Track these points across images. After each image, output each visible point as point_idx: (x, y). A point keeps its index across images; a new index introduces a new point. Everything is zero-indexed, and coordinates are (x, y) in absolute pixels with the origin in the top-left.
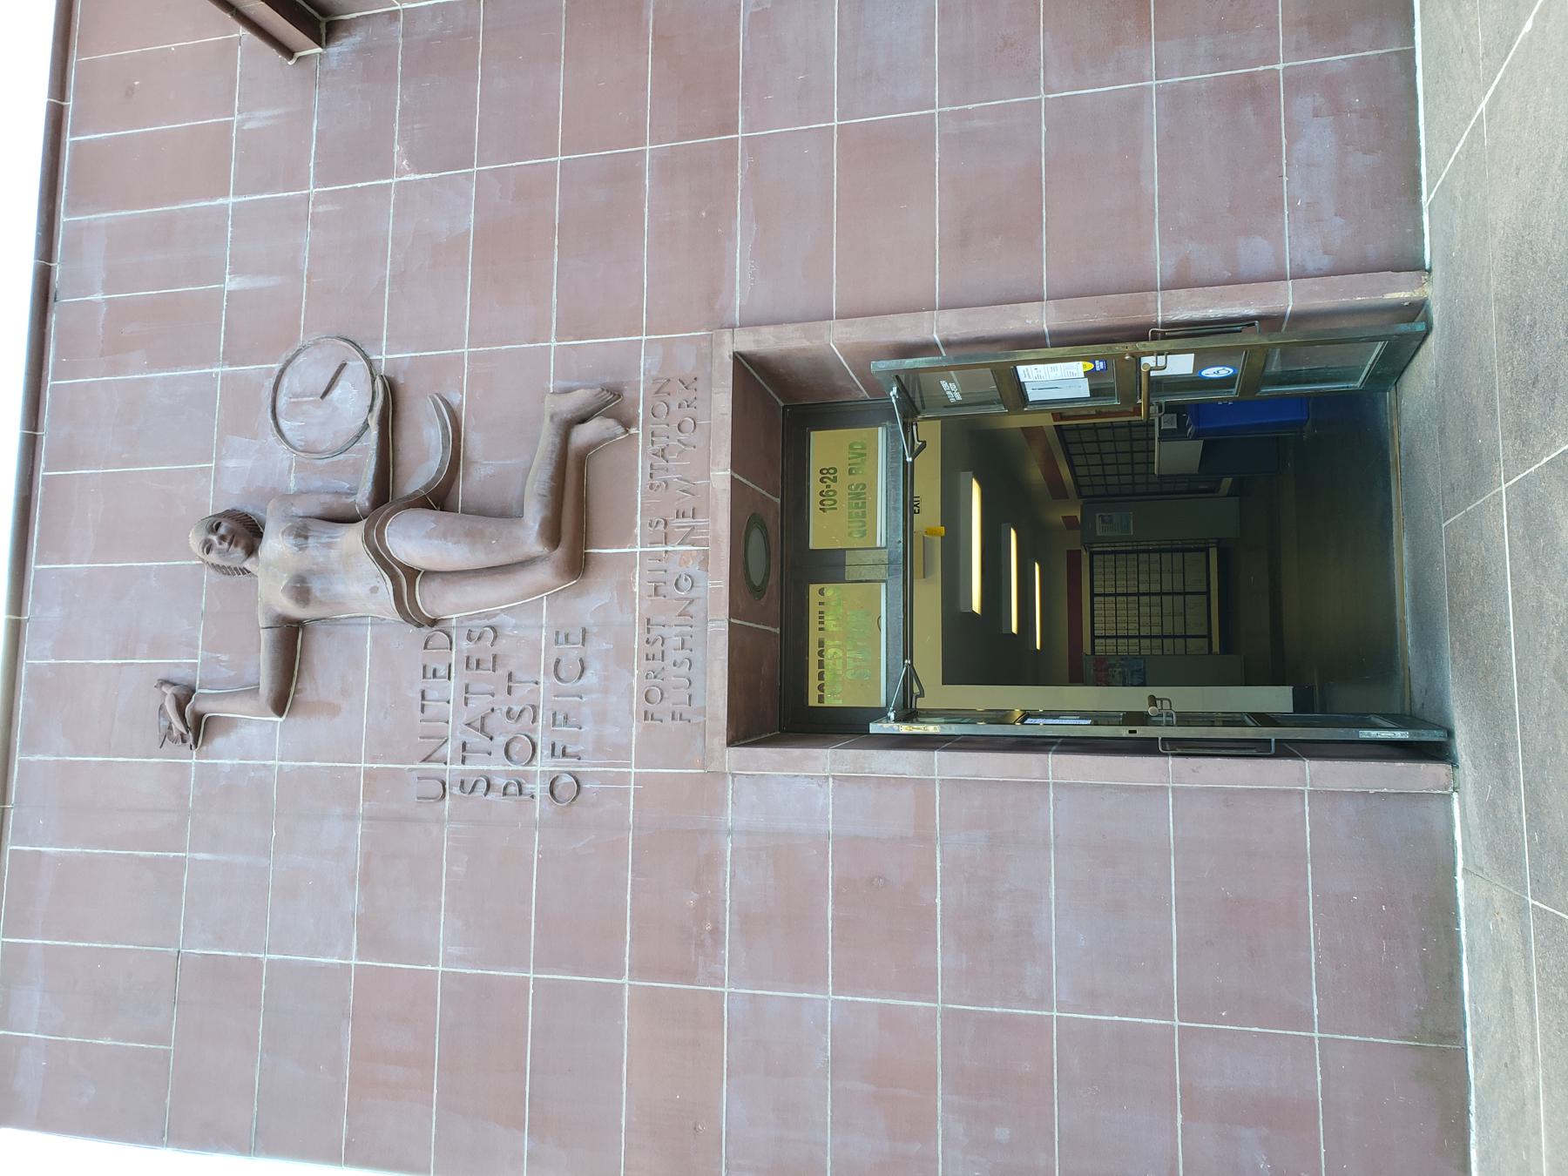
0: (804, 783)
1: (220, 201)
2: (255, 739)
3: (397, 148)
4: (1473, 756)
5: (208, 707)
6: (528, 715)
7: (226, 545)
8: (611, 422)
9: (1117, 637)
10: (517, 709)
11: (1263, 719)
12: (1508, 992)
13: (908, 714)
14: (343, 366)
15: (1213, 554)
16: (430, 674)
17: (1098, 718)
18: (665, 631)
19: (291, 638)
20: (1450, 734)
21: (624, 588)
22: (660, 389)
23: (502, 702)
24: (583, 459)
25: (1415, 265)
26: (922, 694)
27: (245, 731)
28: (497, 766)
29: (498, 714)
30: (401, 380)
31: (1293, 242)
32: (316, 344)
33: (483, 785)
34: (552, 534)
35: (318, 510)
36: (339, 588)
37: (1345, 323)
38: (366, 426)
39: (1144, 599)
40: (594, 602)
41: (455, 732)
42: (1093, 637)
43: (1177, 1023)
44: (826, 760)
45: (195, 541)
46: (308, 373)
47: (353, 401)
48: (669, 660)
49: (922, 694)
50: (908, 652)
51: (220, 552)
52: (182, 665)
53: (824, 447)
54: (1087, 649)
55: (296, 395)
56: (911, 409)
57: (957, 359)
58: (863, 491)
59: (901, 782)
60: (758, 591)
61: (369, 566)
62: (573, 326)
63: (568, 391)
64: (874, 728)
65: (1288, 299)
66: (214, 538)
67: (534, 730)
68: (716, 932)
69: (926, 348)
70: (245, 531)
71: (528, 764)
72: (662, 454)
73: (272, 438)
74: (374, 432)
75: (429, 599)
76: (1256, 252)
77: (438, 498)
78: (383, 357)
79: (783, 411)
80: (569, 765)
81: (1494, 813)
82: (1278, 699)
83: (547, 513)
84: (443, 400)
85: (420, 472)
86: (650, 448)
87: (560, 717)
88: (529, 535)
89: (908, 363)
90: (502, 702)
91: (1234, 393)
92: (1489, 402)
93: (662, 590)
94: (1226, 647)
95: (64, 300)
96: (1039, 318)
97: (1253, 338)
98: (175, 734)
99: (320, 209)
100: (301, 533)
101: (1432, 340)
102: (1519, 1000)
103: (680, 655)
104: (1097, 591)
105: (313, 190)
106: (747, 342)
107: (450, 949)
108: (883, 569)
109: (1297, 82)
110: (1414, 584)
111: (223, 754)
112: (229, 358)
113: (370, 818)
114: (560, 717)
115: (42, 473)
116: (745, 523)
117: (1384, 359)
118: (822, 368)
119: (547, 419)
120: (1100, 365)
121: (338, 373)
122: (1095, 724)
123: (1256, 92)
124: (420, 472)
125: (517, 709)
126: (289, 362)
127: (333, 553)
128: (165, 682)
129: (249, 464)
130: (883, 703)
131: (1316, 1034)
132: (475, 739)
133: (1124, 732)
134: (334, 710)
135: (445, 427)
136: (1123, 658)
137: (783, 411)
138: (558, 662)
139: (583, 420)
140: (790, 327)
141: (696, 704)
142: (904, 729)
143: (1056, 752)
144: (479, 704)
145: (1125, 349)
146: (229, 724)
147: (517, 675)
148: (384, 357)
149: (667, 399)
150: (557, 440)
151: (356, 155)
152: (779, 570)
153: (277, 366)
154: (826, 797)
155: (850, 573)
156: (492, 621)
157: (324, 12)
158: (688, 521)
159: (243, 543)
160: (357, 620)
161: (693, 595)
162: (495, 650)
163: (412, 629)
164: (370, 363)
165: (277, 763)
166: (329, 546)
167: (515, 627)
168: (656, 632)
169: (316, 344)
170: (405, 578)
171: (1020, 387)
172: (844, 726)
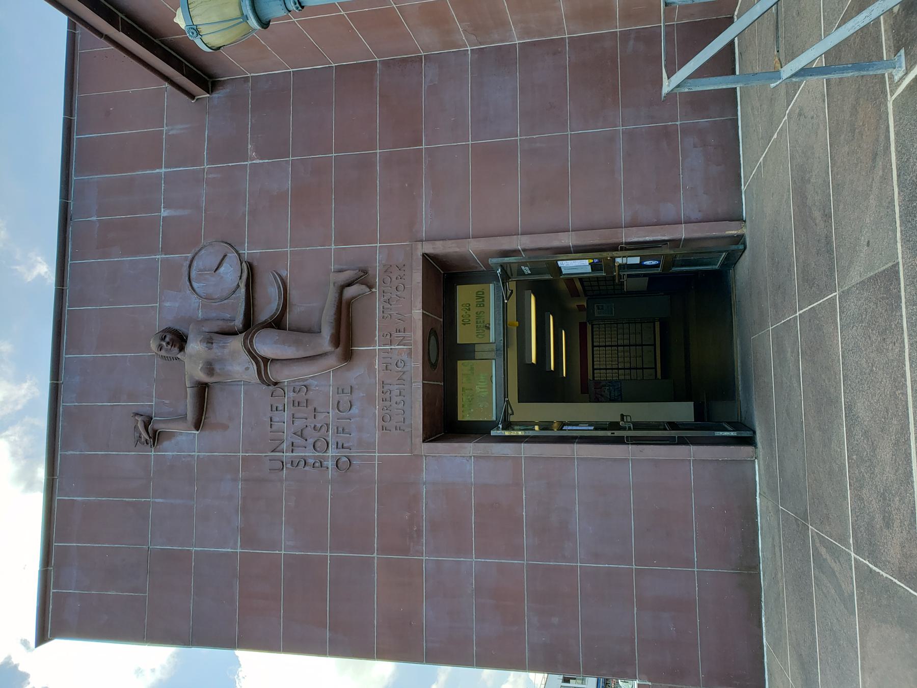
0: (461, 459)
1: (158, 171)
2: (185, 443)
3: (250, 146)
4: (762, 443)
5: (160, 427)
6: (324, 429)
7: (169, 347)
8: (364, 287)
9: (606, 369)
10: (319, 425)
11: (673, 426)
12: (774, 546)
13: (508, 425)
14: (225, 256)
15: (657, 324)
16: (274, 409)
17: (598, 427)
18: (391, 387)
19: (202, 391)
20: (754, 432)
21: (371, 366)
22: (387, 270)
23: (311, 422)
24: (349, 303)
25: (740, 219)
26: (513, 414)
27: (179, 438)
28: (309, 453)
29: (309, 428)
30: (255, 264)
31: (685, 206)
32: (211, 244)
33: (302, 463)
34: (336, 341)
35: (216, 330)
36: (229, 368)
37: (710, 244)
38: (238, 286)
39: (620, 348)
40: (356, 373)
41: (288, 437)
42: (594, 369)
43: (634, 567)
44: (470, 448)
45: (153, 346)
46: (207, 259)
47: (231, 273)
48: (393, 401)
49: (513, 414)
50: (506, 395)
51: (166, 350)
52: (148, 404)
53: (464, 294)
54: (590, 377)
55: (201, 270)
56: (506, 277)
57: (530, 258)
58: (482, 314)
59: (506, 458)
60: (434, 366)
61: (245, 357)
62: (342, 239)
63: (341, 271)
64: (493, 433)
65: (682, 232)
66: (164, 344)
67: (328, 436)
68: (419, 532)
69: (515, 252)
70: (179, 339)
71: (325, 452)
72: (388, 301)
73: (189, 291)
74: (243, 290)
75: (274, 373)
76: (668, 210)
77: (277, 323)
78: (246, 252)
79: (445, 278)
80: (346, 452)
81: (768, 468)
82: (684, 411)
83: (333, 331)
84: (280, 276)
85: (268, 308)
86: (382, 299)
87: (340, 429)
88: (325, 341)
89: (507, 260)
90: (311, 422)
91: (659, 270)
92: (766, 289)
93: (389, 367)
94: (665, 375)
95: (76, 220)
96: (567, 240)
97: (666, 251)
98: (143, 440)
99: (210, 176)
100: (209, 341)
101: (747, 252)
102: (777, 549)
103: (399, 399)
104: (595, 344)
105: (206, 166)
106: (429, 248)
107: (288, 543)
108: (494, 353)
109: (686, 130)
110: (742, 362)
111: (168, 450)
112: (165, 251)
113: (245, 480)
114: (340, 429)
115: (67, 308)
116: (429, 333)
117: (726, 258)
118: (464, 259)
119: (332, 285)
120: (596, 261)
121: (223, 259)
122: (596, 429)
123: (667, 134)
124: (268, 308)
125: (319, 425)
126: (196, 254)
127: (226, 351)
128: (137, 414)
129: (177, 305)
130: (494, 419)
131: (696, 569)
132: (298, 441)
133: (609, 433)
134: (225, 427)
135: (279, 288)
136: (610, 382)
137: (445, 278)
138: (339, 402)
139: (349, 285)
140: (450, 242)
141: (407, 422)
142: (507, 433)
143: (578, 443)
144: (299, 423)
145: (608, 255)
146: (171, 435)
147: (319, 409)
148: (246, 252)
149: (391, 275)
150: (337, 295)
151: (229, 150)
152: (444, 353)
153: (190, 255)
154: (471, 466)
155: (478, 355)
156: (305, 383)
157: (210, 76)
158: (402, 334)
159: (178, 345)
160: (237, 383)
161: (405, 369)
162: (307, 397)
163: (264, 387)
164: (239, 255)
165: (197, 454)
166: (224, 347)
167: (317, 386)
168: (386, 388)
169: (211, 244)
170: (263, 363)
171: (560, 268)
172: (476, 431)
